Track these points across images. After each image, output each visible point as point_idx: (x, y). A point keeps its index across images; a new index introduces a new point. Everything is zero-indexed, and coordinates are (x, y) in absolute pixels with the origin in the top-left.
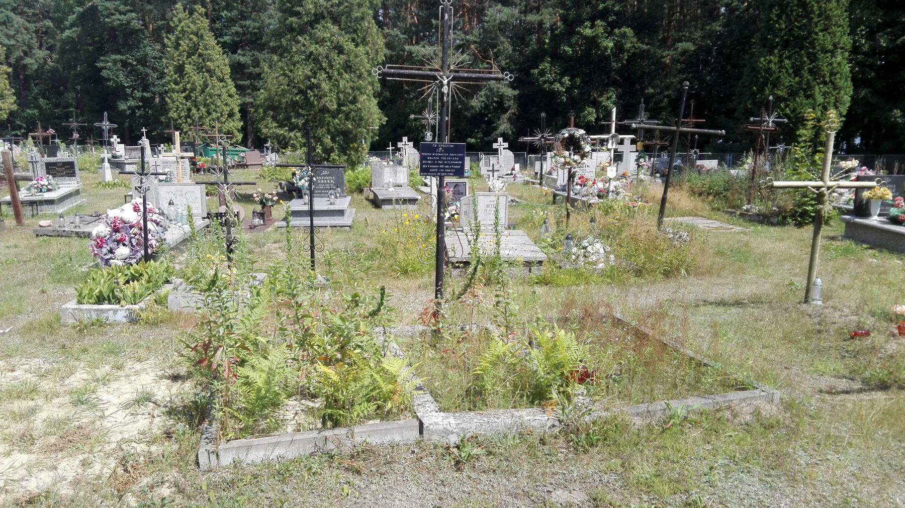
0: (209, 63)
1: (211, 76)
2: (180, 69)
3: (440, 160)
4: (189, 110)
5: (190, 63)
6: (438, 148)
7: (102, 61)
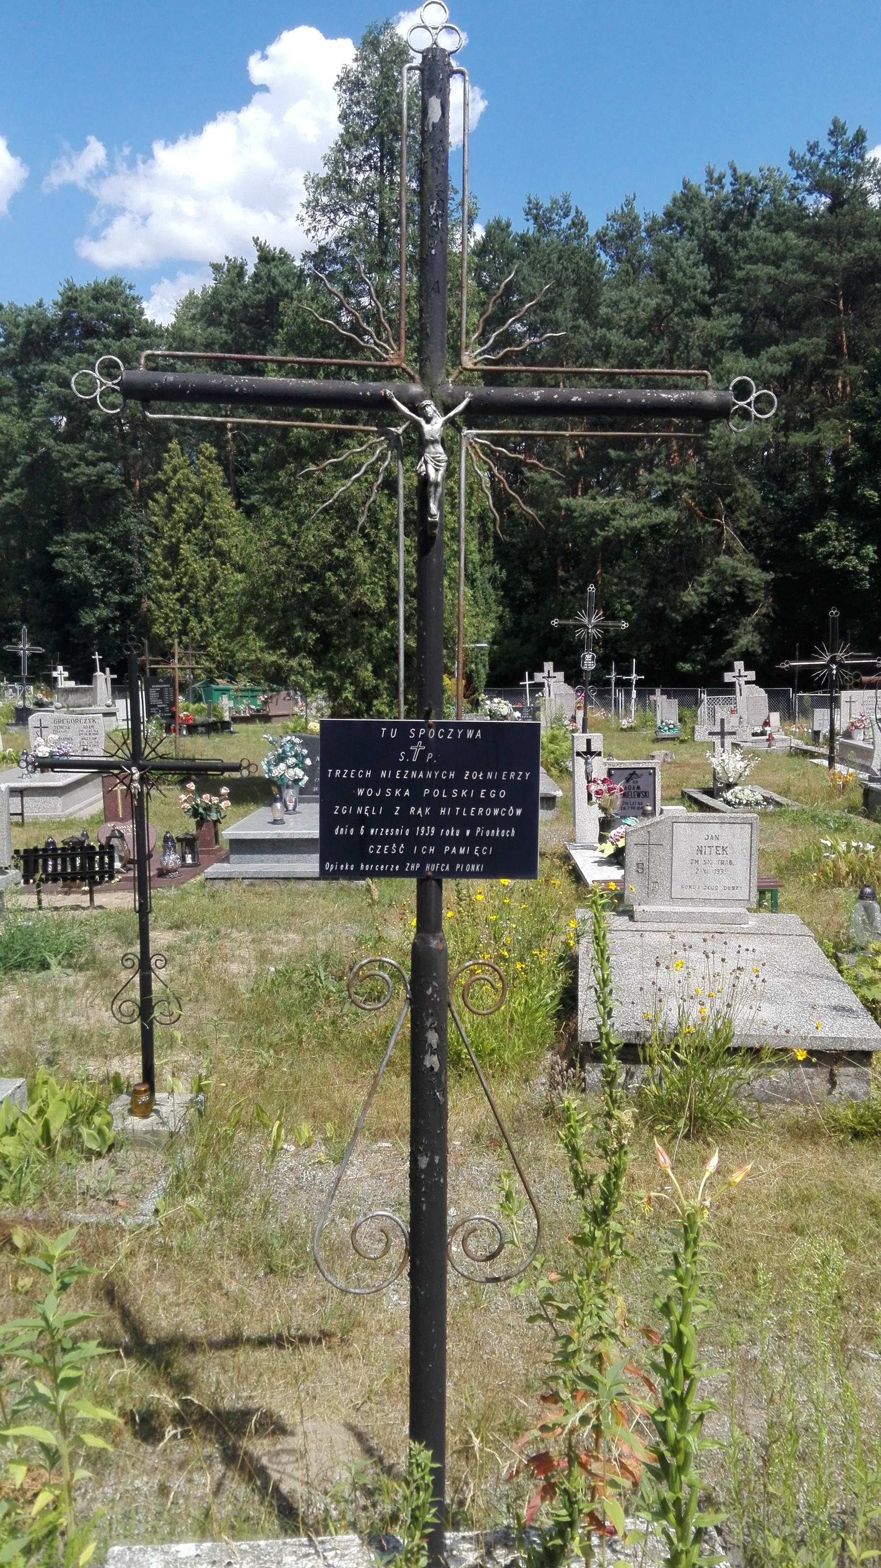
0: (219, 541)
1: (223, 563)
2: (173, 553)
3: (417, 800)
4: (186, 621)
5: (189, 542)
6: (404, 742)
7: (57, 543)
